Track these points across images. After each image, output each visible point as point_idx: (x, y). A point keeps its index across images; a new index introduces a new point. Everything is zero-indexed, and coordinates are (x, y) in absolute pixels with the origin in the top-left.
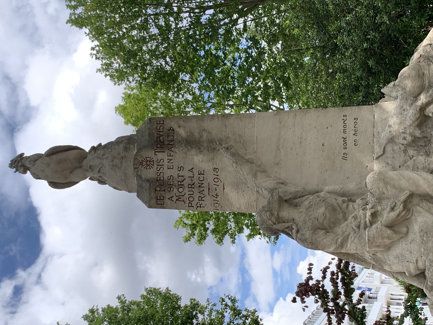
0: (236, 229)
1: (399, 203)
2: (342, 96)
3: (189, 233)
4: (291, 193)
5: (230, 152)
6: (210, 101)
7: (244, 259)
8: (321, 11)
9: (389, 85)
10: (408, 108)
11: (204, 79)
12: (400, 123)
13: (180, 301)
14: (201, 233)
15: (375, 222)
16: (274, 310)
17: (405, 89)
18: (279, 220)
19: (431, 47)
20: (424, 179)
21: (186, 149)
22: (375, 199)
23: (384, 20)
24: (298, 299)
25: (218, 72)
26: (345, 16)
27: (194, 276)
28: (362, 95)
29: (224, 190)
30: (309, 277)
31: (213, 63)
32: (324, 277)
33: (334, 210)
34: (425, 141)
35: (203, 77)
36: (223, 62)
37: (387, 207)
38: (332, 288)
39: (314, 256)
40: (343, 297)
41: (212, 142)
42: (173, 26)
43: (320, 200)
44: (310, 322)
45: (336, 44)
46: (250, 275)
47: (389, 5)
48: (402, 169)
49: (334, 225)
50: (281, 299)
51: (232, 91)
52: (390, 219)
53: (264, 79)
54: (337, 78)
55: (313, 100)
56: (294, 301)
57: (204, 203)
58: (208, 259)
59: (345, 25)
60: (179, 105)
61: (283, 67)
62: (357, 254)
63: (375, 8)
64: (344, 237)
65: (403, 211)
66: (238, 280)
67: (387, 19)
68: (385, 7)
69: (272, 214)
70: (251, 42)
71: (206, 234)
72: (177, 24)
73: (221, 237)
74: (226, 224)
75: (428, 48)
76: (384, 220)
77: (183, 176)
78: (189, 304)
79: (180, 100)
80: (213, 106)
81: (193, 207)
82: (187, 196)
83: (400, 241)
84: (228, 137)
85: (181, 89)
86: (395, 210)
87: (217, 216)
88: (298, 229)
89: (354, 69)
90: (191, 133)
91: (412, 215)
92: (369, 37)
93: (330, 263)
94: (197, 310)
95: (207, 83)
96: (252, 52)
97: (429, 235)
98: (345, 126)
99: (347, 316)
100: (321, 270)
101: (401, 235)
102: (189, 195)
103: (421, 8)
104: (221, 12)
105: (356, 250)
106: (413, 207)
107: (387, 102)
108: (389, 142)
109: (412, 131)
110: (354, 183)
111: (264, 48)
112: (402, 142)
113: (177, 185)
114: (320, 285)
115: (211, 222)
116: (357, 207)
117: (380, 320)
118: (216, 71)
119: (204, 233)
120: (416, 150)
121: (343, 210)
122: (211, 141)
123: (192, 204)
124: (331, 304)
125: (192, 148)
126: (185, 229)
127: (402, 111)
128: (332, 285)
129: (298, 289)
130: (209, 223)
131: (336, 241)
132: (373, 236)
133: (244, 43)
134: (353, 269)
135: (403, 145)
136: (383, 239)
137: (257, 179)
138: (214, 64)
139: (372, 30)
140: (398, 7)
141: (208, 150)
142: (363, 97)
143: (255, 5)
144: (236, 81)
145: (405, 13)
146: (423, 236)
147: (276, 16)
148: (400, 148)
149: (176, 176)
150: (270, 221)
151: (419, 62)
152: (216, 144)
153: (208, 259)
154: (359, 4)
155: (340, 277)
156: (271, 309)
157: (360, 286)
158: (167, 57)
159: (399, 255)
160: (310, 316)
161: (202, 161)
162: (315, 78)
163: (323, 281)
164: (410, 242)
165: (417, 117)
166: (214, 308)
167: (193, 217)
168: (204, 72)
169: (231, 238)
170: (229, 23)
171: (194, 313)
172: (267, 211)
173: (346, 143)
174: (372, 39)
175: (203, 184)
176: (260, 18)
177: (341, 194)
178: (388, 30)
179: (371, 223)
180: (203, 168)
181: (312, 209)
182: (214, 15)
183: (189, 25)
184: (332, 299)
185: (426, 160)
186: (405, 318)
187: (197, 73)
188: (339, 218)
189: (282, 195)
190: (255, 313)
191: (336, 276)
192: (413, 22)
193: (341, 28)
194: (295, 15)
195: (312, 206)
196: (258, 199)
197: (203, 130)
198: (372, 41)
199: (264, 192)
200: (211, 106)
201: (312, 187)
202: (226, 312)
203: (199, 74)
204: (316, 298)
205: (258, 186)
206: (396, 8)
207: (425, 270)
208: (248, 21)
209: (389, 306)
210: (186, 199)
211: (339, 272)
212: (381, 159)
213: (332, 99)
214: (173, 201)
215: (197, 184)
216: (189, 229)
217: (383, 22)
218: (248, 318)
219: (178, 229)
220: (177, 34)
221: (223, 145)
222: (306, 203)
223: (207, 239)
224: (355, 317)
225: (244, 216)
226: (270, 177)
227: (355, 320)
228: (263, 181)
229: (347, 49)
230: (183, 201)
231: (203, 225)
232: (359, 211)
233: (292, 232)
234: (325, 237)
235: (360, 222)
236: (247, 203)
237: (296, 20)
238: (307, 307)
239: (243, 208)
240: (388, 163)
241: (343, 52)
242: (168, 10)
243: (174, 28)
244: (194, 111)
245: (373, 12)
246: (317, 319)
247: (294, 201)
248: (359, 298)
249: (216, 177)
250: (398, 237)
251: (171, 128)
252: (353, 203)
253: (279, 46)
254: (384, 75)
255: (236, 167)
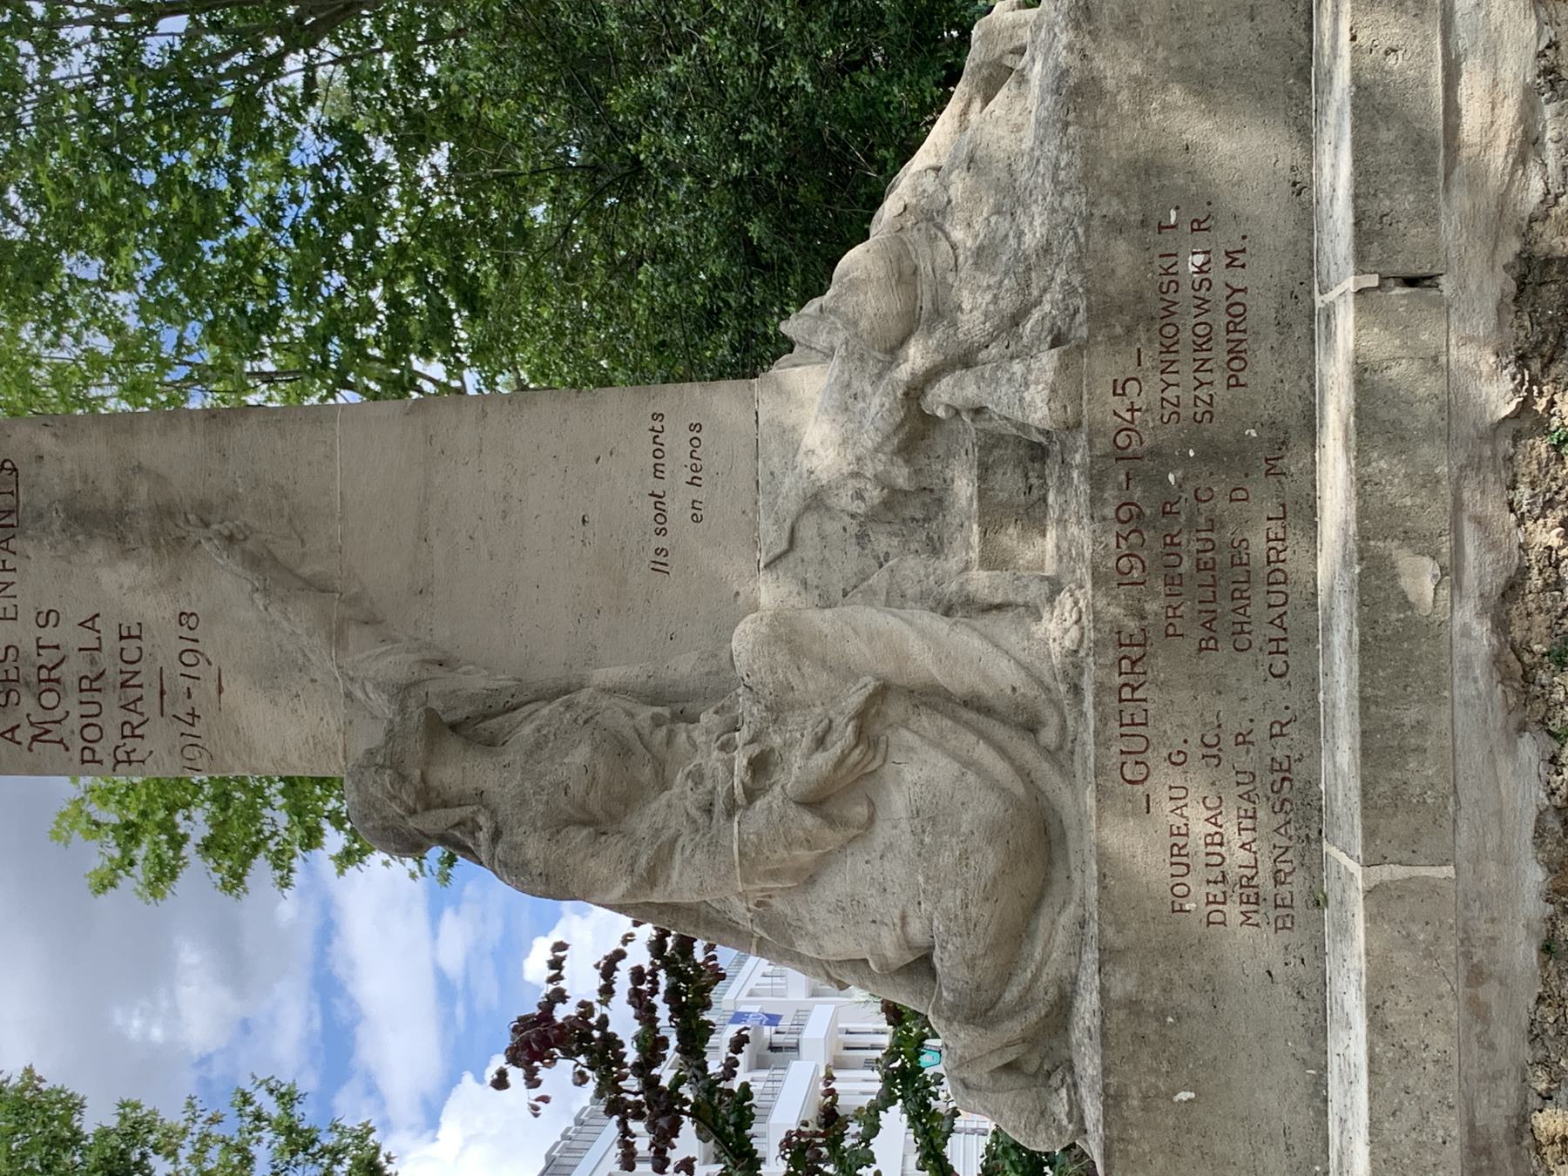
0: (293, 833)
1: (840, 721)
2: (663, 343)
3: (111, 859)
4: (471, 698)
5: (243, 551)
6: (186, 358)
7: (329, 942)
8: (580, 40)
9: (806, 310)
10: (869, 389)
11: (157, 276)
12: (844, 442)
13: (80, 1113)
14: (158, 856)
15: (765, 791)
16: (442, 1119)
17: (856, 324)
18: (430, 799)
19: (937, 176)
20: (923, 633)
21: (68, 544)
22: (762, 707)
23: (798, 80)
24: (516, 1075)
25: (211, 248)
26: (663, 62)
27: (136, 1023)
28: (730, 341)
29: (220, 693)
30: (555, 991)
31: (190, 215)
32: (607, 991)
33: (623, 751)
34: (924, 504)
35: (153, 268)
36: (231, 213)
37: (802, 735)
38: (636, 1027)
39: (584, 917)
40: (671, 1054)
41: (171, 515)
42: (33, 71)
43: (575, 721)
44: (569, 1150)
45: (635, 159)
46: (351, 1001)
47: (812, 25)
48: (854, 599)
49: (623, 807)
50: (468, 1078)
51: (268, 321)
52: (813, 778)
53: (389, 282)
54: (641, 281)
55: (563, 359)
56: (501, 1082)
57: (141, 748)
58: (191, 956)
59: (664, 94)
60: (59, 376)
61: (445, 236)
62: (704, 905)
63: (767, 37)
64: (659, 847)
65: (856, 746)
66: (310, 1019)
67: (807, 76)
68: (800, 33)
69: (403, 778)
70: (336, 143)
71: (177, 857)
72: (46, 67)
73: (236, 866)
74: (256, 817)
75: (929, 182)
76: (793, 779)
77: (57, 647)
78: (112, 1122)
79: (65, 354)
80: (201, 377)
81: (100, 762)
82: (74, 722)
83: (849, 851)
84: (233, 498)
85: (68, 313)
86: (829, 745)
87: (220, 790)
88: (496, 828)
89: (699, 250)
90: (86, 482)
91: (885, 761)
92: (748, 137)
93: (625, 941)
94: (145, 1143)
95: (170, 290)
96: (339, 179)
97: (940, 828)
98: (659, 454)
99: (687, 1121)
100: (597, 966)
101: (855, 832)
102: (82, 716)
103: (921, 39)
104: (216, 27)
105: (700, 891)
106: (889, 732)
107: (798, 370)
108: (807, 508)
109: (881, 468)
110: (694, 655)
111: (383, 167)
112: (849, 508)
113: (34, 680)
114: (593, 1021)
115: (198, 814)
116: (703, 739)
117: (803, 1129)
118: (206, 245)
119: (171, 854)
120: (896, 535)
121: (654, 750)
122: (165, 512)
123: (93, 751)
124: (632, 1083)
125: (91, 536)
126: (96, 842)
127: (846, 401)
128: (636, 1018)
129: (513, 1039)
130: (188, 818)
131: (632, 865)
132: (755, 840)
133: (309, 148)
134: (710, 954)
135: (853, 516)
136: (789, 846)
137: (345, 649)
138: (196, 218)
139: (757, 113)
140: (844, 34)
141: (156, 547)
142: (734, 350)
143: (348, 7)
144: (281, 283)
145: (867, 55)
146: (924, 832)
147: (427, 51)
148: (845, 529)
149: (29, 646)
150: (393, 805)
151: (902, 228)
152: (187, 521)
153: (191, 956)
154: (713, 18)
155: (662, 987)
156: (431, 1118)
157: (743, 1009)
158: (12, 188)
159: (847, 903)
160: (568, 1129)
161: (132, 589)
162: (567, 278)
163: (604, 1003)
164: (879, 854)
165: (898, 420)
166: (215, 1130)
167: (127, 795)
168: (159, 250)
169: (276, 867)
170: (251, 69)
171: (135, 1156)
172: (382, 767)
173: (662, 513)
174: (758, 145)
175: (137, 673)
176: (368, 56)
177: (647, 696)
178: (811, 114)
179: (751, 795)
180: (136, 613)
181: (546, 753)
182: (191, 37)
183: (97, 74)
184: (636, 1066)
185: (931, 570)
186: (882, 1114)
187: (128, 254)
188: (642, 779)
189: (437, 704)
190: (367, 1138)
191: (649, 982)
192: (896, 90)
193: (650, 102)
194: (488, 47)
195: (547, 743)
196: (350, 723)
197: (133, 469)
198: (757, 152)
199: (371, 695)
200: (189, 378)
201: (547, 672)
202: (259, 1141)
203: (138, 256)
204: (579, 1068)
205: (351, 673)
206: (836, 38)
207: (934, 947)
208: (324, 64)
209: (830, 1078)
210: (73, 732)
211: (660, 967)
212: (781, 566)
213: (627, 355)
214: (19, 743)
215: (114, 677)
216: (113, 843)
217: (792, 87)
218: (341, 1156)
219: (66, 844)
220: (46, 101)
221: (215, 527)
222: (527, 730)
223: (183, 875)
224: (716, 1124)
225: (325, 786)
226: (395, 641)
227: (716, 1133)
228: (369, 657)
229: (675, 175)
230: (61, 742)
231: (167, 827)
232: (709, 755)
233: (474, 838)
234: (591, 850)
235: (712, 792)
236: (311, 740)
237: (491, 68)
238: (545, 1099)
239: (293, 758)
240: (805, 583)
241: (661, 189)
242: (8, 11)
243: (35, 82)
244: (120, 396)
245: (761, 48)
246: (592, 1137)
247: (482, 725)
248: (731, 1055)
249: (191, 645)
250: (839, 836)
251: (5, 461)
252: (691, 726)
253: (441, 157)
254: (802, 270)
255: (266, 609)
